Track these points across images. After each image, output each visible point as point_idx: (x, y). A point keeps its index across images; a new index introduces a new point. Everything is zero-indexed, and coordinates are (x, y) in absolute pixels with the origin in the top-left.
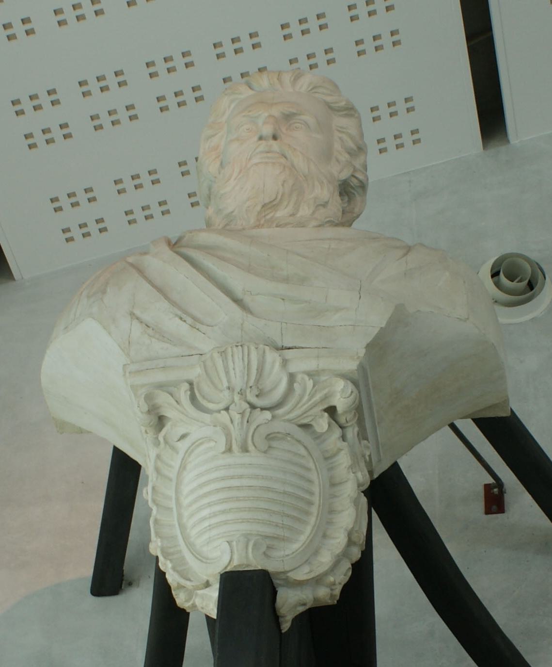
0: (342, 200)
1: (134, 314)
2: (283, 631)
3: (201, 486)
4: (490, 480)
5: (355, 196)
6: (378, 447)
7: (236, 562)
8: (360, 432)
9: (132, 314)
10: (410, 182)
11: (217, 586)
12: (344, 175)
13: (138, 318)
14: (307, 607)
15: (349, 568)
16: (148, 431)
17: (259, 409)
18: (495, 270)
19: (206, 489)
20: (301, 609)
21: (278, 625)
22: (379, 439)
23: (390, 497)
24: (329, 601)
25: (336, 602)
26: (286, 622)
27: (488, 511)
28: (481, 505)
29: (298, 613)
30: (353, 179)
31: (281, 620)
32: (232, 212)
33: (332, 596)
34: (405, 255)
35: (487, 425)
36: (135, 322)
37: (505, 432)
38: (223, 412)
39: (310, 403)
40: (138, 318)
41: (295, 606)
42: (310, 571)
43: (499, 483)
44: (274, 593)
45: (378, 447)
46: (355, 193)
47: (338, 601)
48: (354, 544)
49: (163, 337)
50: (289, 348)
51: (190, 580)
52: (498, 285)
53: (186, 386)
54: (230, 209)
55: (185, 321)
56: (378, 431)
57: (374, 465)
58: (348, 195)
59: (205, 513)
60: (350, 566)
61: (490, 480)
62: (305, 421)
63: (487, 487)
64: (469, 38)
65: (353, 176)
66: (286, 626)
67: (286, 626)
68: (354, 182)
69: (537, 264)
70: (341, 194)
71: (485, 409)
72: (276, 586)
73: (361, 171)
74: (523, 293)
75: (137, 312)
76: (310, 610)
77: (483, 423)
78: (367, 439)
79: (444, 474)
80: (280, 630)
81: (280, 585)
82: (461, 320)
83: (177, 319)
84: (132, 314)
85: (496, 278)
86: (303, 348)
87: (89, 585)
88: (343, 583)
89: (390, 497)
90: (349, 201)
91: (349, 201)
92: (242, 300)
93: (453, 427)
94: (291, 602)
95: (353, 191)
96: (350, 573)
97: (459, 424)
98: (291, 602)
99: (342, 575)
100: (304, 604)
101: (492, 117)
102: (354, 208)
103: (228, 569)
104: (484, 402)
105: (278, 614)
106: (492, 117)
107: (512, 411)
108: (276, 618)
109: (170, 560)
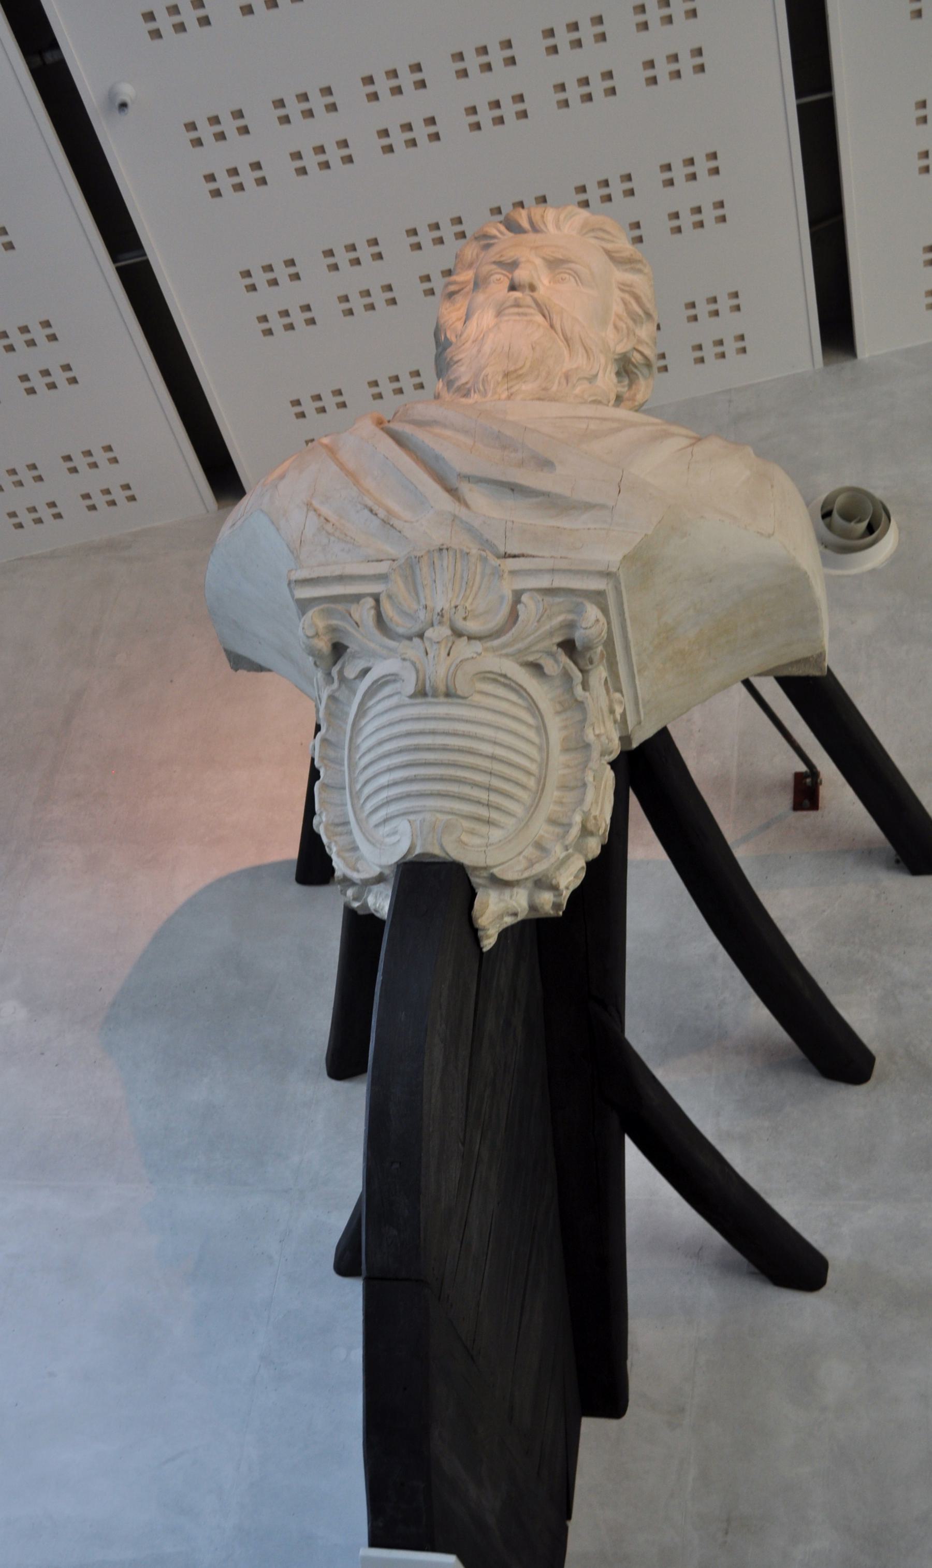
0: (619, 382)
1: (311, 504)
2: (485, 950)
3: (380, 743)
4: (802, 768)
5: (638, 378)
6: (636, 704)
7: (418, 851)
8: (609, 679)
9: (309, 505)
10: (730, 401)
11: (392, 881)
12: (621, 348)
13: (315, 510)
14: (520, 918)
15: (583, 868)
16: (318, 663)
17: (466, 638)
18: (825, 510)
19: (387, 747)
20: (509, 921)
21: (477, 941)
22: (639, 691)
23: (651, 773)
24: (552, 912)
25: (561, 913)
26: (488, 937)
27: (798, 806)
28: (787, 799)
29: (505, 926)
30: (636, 354)
31: (480, 933)
32: (467, 383)
33: (556, 906)
34: (692, 445)
35: (794, 686)
36: (311, 513)
37: (819, 699)
38: (416, 640)
39: (537, 634)
40: (315, 510)
41: (501, 916)
42: (523, 864)
43: (813, 773)
44: (473, 894)
45: (636, 704)
46: (640, 375)
47: (564, 913)
48: (592, 834)
49: (346, 535)
50: (515, 556)
51: (358, 871)
52: (829, 527)
53: (371, 602)
54: (463, 380)
55: (376, 514)
56: (637, 682)
57: (630, 728)
58: (629, 376)
59: (384, 780)
60: (584, 865)
61: (802, 768)
62: (531, 658)
63: (798, 777)
64: (812, 223)
65: (635, 349)
66: (488, 943)
67: (488, 943)
68: (636, 358)
69: (882, 503)
70: (618, 374)
71: (791, 664)
72: (474, 886)
73: (647, 344)
74: (863, 536)
75: (315, 503)
76: (523, 923)
77: (789, 684)
78: (619, 690)
79: (736, 752)
80: (481, 949)
81: (480, 885)
82: (762, 534)
83: (366, 512)
84: (309, 505)
85: (828, 519)
86: (533, 557)
87: (294, 869)
88: (572, 889)
89: (651, 773)
90: (630, 386)
91: (630, 386)
92: (456, 490)
93: (747, 683)
94: (495, 913)
95: (635, 371)
96: (583, 875)
97: (756, 682)
98: (495, 913)
99: (570, 878)
100: (515, 914)
101: (837, 327)
102: (635, 395)
103: (410, 858)
104: (788, 651)
105: (476, 926)
106: (837, 327)
107: (829, 669)
108: (474, 933)
109: (336, 842)
